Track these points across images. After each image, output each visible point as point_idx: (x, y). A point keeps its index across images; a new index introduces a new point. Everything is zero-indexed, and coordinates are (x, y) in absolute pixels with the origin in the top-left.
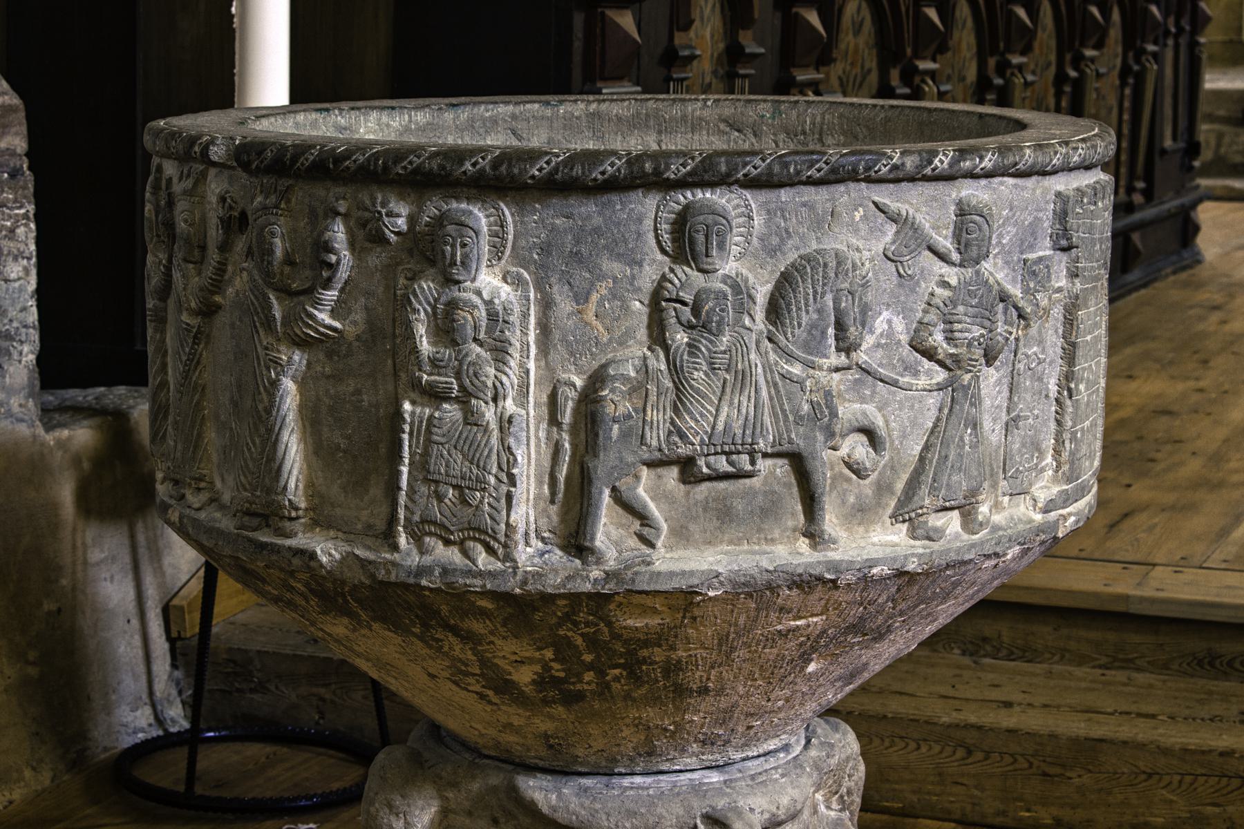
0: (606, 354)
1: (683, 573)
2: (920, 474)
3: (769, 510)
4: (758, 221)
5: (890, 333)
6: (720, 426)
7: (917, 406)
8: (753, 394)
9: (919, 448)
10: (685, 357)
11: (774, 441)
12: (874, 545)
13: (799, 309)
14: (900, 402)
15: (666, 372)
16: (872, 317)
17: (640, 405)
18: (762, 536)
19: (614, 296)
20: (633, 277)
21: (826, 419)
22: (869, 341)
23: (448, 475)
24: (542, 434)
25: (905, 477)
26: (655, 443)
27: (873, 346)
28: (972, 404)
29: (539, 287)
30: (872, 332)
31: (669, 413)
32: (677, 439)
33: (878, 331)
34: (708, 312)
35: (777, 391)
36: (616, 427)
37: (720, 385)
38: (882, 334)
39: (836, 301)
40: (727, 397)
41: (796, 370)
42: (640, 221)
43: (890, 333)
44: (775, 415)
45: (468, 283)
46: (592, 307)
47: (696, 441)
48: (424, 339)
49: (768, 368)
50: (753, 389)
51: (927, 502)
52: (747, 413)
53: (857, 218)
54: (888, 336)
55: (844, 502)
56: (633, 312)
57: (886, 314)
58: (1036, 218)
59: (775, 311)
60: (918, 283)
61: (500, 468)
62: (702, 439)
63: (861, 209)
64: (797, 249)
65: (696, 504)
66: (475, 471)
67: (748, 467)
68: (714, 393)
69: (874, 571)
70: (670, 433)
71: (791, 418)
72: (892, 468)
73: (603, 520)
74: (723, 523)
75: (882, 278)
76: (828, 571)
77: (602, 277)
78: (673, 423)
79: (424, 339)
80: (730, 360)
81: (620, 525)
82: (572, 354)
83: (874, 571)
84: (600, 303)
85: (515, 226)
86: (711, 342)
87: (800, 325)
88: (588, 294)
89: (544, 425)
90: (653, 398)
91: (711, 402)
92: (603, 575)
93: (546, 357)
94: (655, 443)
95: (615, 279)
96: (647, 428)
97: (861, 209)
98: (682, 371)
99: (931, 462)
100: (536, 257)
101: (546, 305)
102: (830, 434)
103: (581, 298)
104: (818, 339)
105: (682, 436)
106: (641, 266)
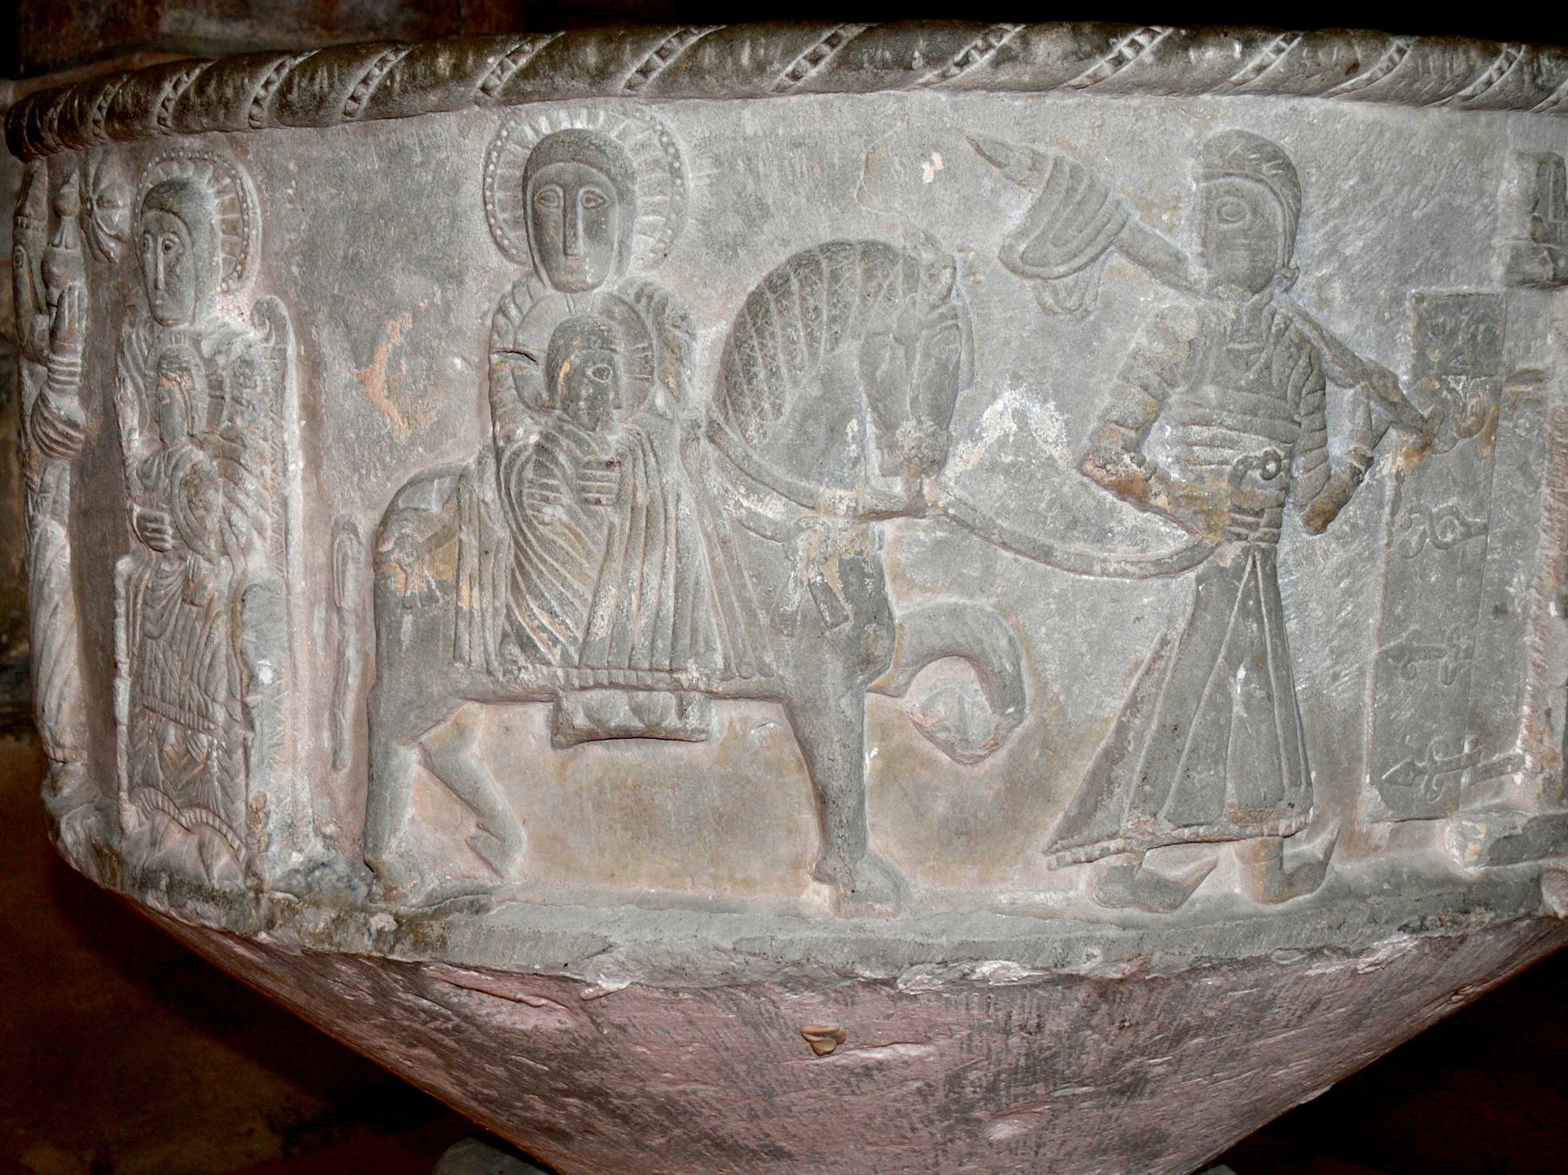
0: (407, 470)
1: (536, 937)
2: (1114, 762)
3: (731, 817)
4: (695, 181)
5: (1025, 438)
6: (602, 628)
7: (1106, 608)
8: (671, 560)
9: (1119, 704)
10: (529, 474)
11: (727, 667)
12: (996, 910)
13: (773, 373)
14: (1061, 598)
15: (495, 507)
16: (972, 401)
17: (449, 577)
18: (724, 872)
19: (416, 346)
20: (448, 307)
21: (847, 626)
22: (964, 458)
23: (163, 700)
24: (318, 629)
25: (1085, 765)
26: (477, 658)
27: (980, 466)
28: (1245, 612)
29: (303, 336)
30: (974, 437)
31: (505, 594)
32: (516, 651)
33: (991, 436)
34: (568, 378)
35: (730, 557)
36: (408, 619)
37: (601, 537)
38: (1002, 443)
39: (869, 360)
40: (617, 565)
41: (773, 509)
42: (455, 185)
43: (1025, 438)
44: (728, 610)
45: (185, 326)
46: (380, 369)
47: (555, 656)
48: (136, 436)
49: (708, 504)
50: (671, 549)
51: (1127, 825)
52: (660, 603)
53: (928, 177)
54: (1017, 449)
55: (920, 813)
56: (450, 380)
57: (1009, 398)
58: (1446, 206)
59: (734, 376)
60: (1096, 327)
61: (231, 694)
62: (565, 655)
63: (936, 157)
64: (785, 243)
65: (578, 794)
66: (197, 694)
67: (672, 721)
68: (588, 554)
69: (986, 968)
70: (505, 635)
71: (763, 618)
72: (1045, 745)
73: (410, 812)
74: (637, 838)
75: (997, 313)
76: (865, 960)
77: (393, 309)
78: (509, 616)
79: (136, 436)
80: (622, 482)
81: (439, 825)
82: (356, 470)
83: (986, 968)
84: (393, 365)
85: (264, 212)
86: (580, 442)
87: (778, 410)
88: (374, 343)
89: (320, 612)
90: (471, 561)
91: (583, 576)
92: (393, 926)
93: (317, 474)
94: (477, 658)
95: (416, 315)
96: (462, 625)
97: (936, 157)
98: (521, 503)
99: (1140, 736)
100: (295, 270)
101: (314, 366)
102: (864, 662)
103: (362, 353)
104: (821, 444)
105: (526, 645)
106: (461, 283)
